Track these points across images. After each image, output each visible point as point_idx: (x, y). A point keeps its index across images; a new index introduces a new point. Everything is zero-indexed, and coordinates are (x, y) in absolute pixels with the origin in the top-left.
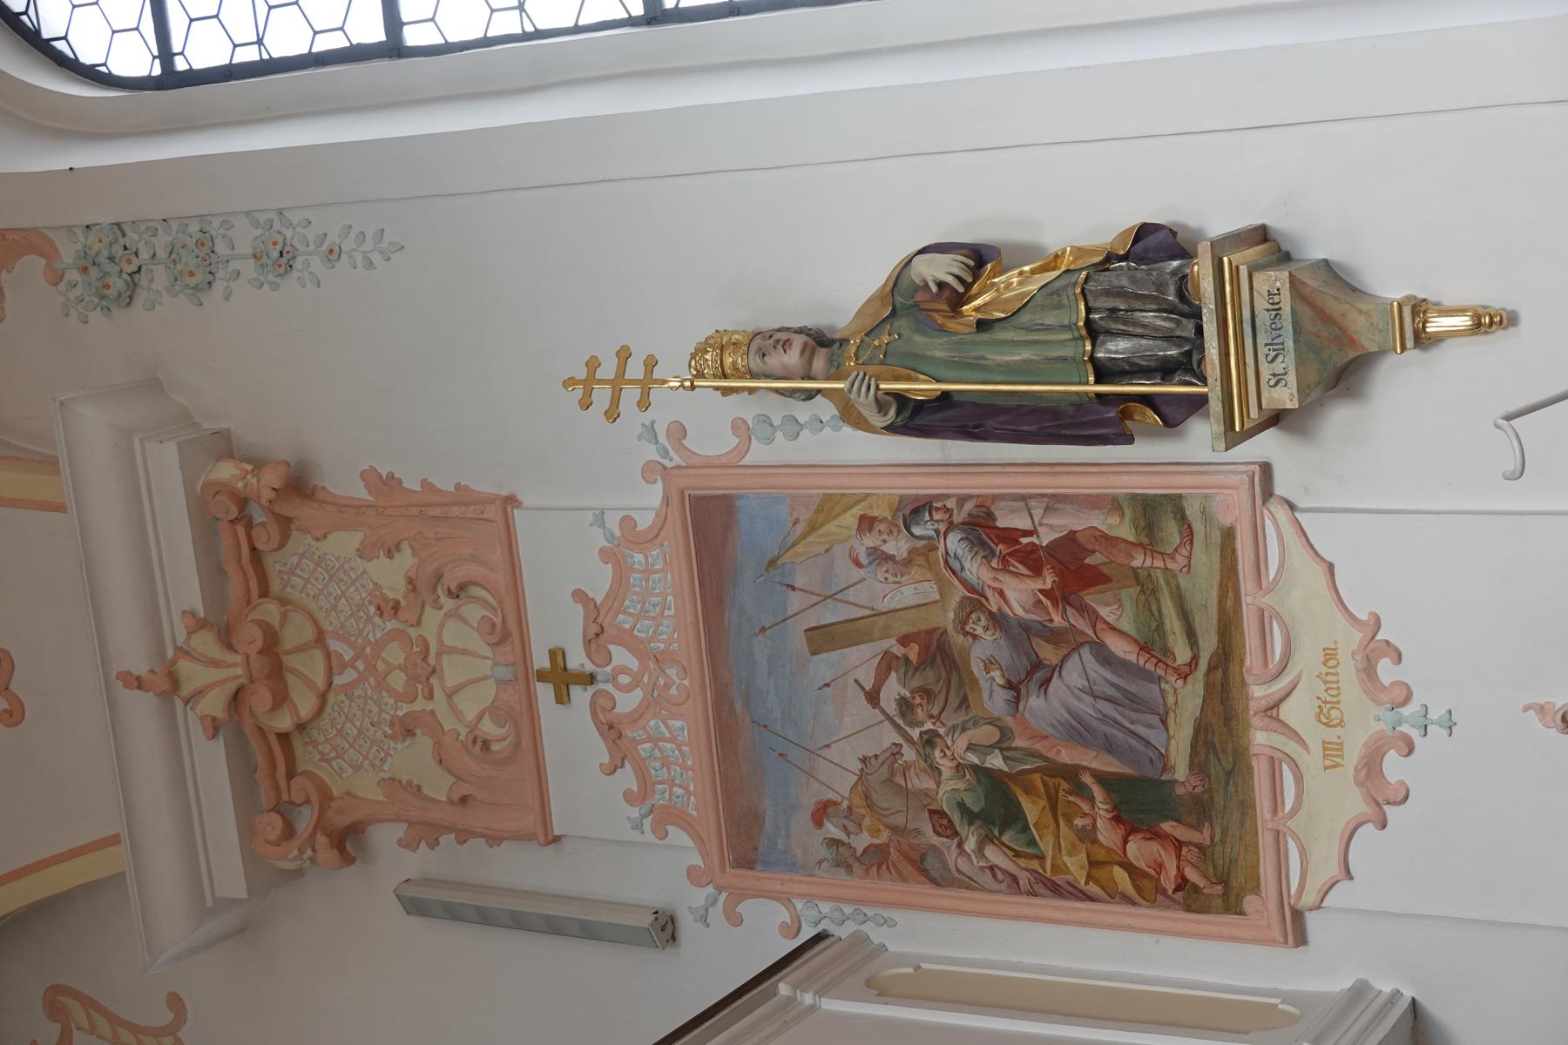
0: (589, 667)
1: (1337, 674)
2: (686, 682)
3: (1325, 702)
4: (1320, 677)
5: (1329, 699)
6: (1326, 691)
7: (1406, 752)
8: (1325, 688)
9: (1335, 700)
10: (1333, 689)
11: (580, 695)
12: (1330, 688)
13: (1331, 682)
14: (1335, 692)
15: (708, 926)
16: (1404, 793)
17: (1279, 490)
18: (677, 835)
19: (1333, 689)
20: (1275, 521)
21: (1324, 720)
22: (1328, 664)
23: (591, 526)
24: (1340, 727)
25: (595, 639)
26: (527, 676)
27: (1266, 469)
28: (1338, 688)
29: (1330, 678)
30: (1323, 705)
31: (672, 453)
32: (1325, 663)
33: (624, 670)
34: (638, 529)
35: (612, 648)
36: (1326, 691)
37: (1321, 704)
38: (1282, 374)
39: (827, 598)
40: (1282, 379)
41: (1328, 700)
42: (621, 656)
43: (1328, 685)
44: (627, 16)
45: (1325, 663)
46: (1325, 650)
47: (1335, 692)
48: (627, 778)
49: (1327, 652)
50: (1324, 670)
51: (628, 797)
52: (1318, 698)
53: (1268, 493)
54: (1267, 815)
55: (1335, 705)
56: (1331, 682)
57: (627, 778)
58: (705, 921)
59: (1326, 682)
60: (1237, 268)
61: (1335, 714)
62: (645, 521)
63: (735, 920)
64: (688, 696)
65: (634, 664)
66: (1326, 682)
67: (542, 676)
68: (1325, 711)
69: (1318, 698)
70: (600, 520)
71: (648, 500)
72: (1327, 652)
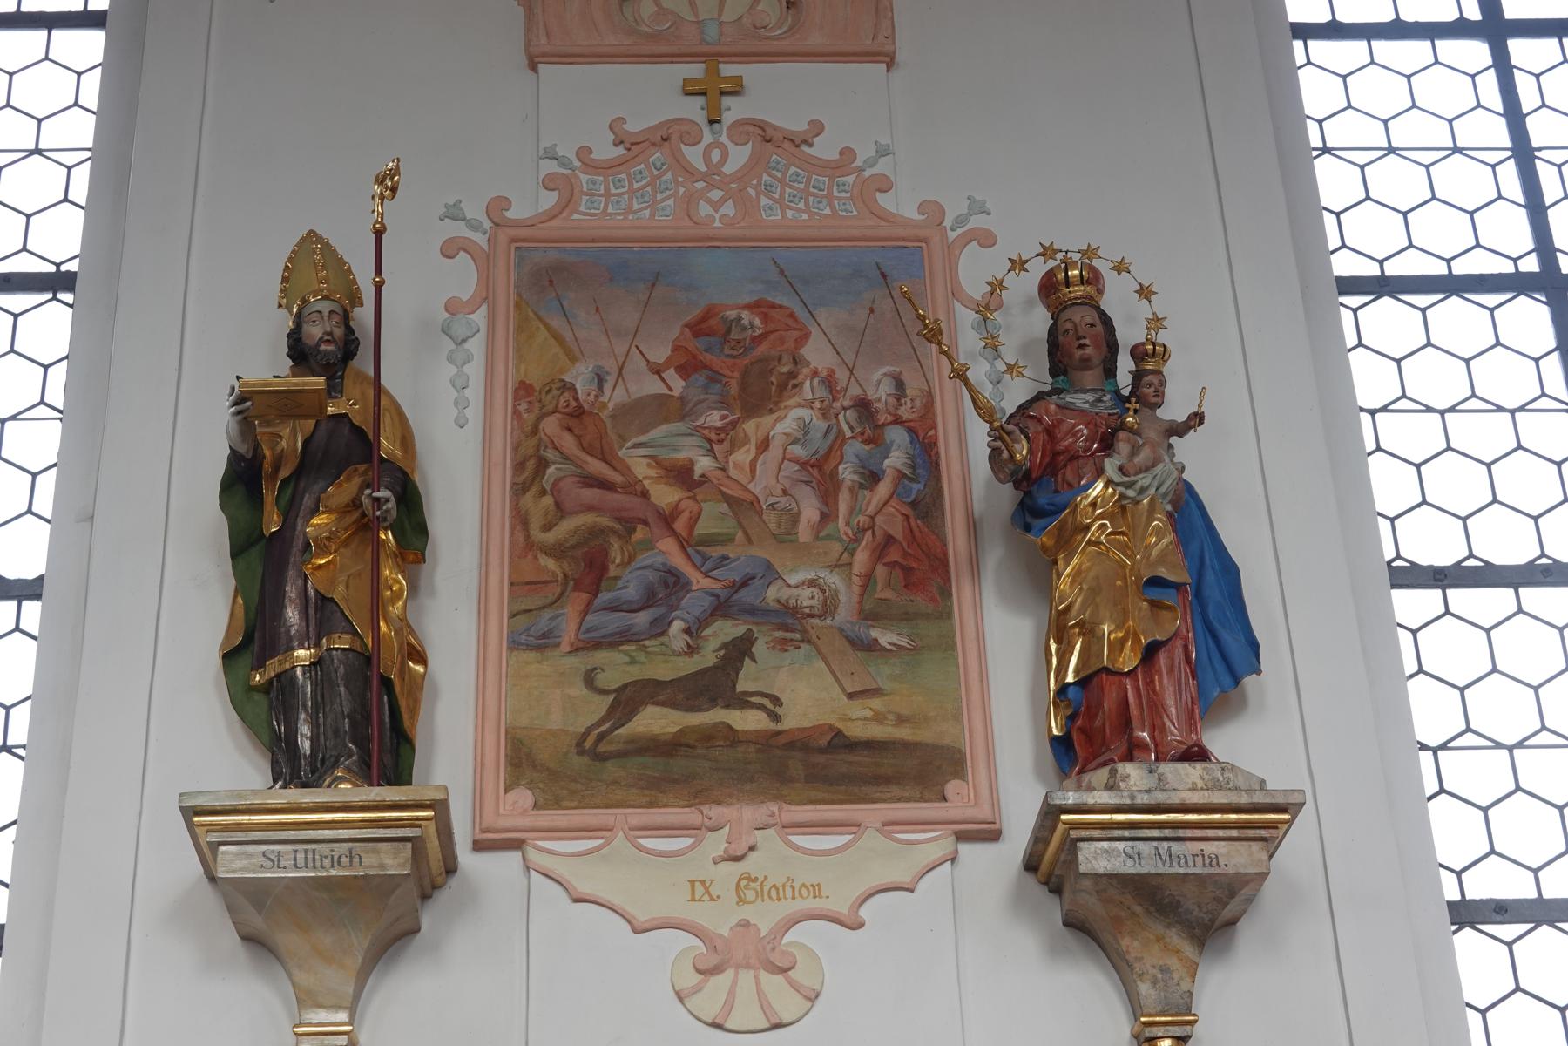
0: (729, 118)
1: (794, 898)
2: (717, 224)
3: (762, 885)
4: (789, 880)
5: (766, 889)
6: (774, 886)
7: (701, 967)
8: (778, 885)
9: (766, 896)
10: (778, 893)
11: (694, 109)
12: (777, 890)
13: (784, 891)
14: (774, 896)
15: (441, 220)
16: (790, 965)
17: (964, 848)
18: (549, 200)
19: (778, 893)
20: (934, 844)
21: (743, 883)
22: (803, 888)
23: (876, 143)
24: (737, 900)
25: (762, 133)
26: (711, 58)
27: (993, 836)
28: (779, 899)
29: (789, 891)
30: (758, 883)
31: (960, 231)
32: (804, 885)
33: (725, 156)
34: (878, 194)
35: (749, 147)
36: (774, 886)
37: (760, 880)
38: (278, 864)
39: (851, 371)
40: (274, 864)
41: (765, 888)
42: (739, 156)
43: (781, 889)
44: (1547, 204)
45: (804, 885)
46: (819, 885)
47: (774, 896)
48: (605, 150)
49: (817, 888)
50: (797, 885)
51: (584, 152)
52: (766, 878)
53: (962, 837)
54: (634, 821)
55: (759, 894)
56: (784, 891)
57: (605, 150)
58: (446, 217)
59: (784, 886)
60: (1277, 828)
61: (750, 895)
62: (885, 201)
63: (450, 250)
64: (695, 223)
65: (728, 169)
66: (784, 886)
67: (712, 71)
68: (753, 885)
69: (766, 878)
70: (883, 151)
71: (902, 204)
72: (817, 888)
